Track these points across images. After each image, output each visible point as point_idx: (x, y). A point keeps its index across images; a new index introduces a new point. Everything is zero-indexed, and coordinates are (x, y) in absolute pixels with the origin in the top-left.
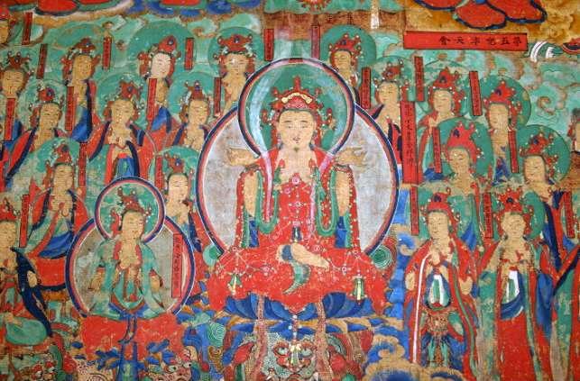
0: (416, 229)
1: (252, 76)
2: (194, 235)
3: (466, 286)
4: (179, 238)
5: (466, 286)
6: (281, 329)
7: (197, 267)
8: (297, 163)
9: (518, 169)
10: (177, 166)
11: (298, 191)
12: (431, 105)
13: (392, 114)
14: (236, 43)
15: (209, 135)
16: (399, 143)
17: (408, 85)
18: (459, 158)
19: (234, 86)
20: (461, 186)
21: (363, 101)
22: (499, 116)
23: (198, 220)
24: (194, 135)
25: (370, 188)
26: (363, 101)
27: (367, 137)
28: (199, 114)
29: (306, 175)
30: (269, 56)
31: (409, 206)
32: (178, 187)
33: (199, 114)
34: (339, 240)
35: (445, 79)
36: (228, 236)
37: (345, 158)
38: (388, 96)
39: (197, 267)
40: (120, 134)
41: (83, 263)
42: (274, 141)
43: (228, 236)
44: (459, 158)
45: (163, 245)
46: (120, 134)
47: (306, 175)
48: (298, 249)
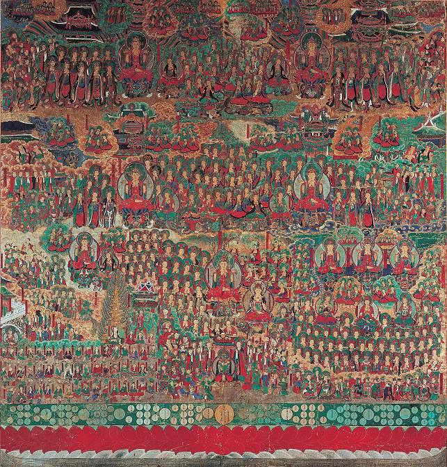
0: (334, 196)
1: (303, 165)
2: (293, 197)
3: (344, 206)
4: (290, 197)
5: (344, 206)
6: (309, 214)
7: (294, 204)
8: (405, 254)
9: (354, 184)
10: (289, 184)
11: (313, 188)
12: (41, 411)
13: (330, 173)
14: (300, 158)
15: (295, 178)
16: (331, 179)
17: (186, 348)
18: (343, 182)
19: (300, 167)
20: (344, 187)
21: (326, 172)
22: (351, 173)
23: (293, 193)
24: (292, 177)
25: (326, 188)
26: (326, 172)
27: (325, 178)
28: (293, 173)
29: (313, 185)
30: (306, 162)
31: (334, 192)
32: (289, 188)
33: (293, 173)
34: (320, 196)
35: (341, 166)
36: (299, 197)
37: (321, 182)
38: (330, 169)
39: (294, 204)
40: (277, 178)
41: (272, 203)
42: (307, 179)
43: (299, 197)
44: (343, 182)
45: (287, 199)
46: (277, 178)
47: (313, 185)
48: (312, 199)
